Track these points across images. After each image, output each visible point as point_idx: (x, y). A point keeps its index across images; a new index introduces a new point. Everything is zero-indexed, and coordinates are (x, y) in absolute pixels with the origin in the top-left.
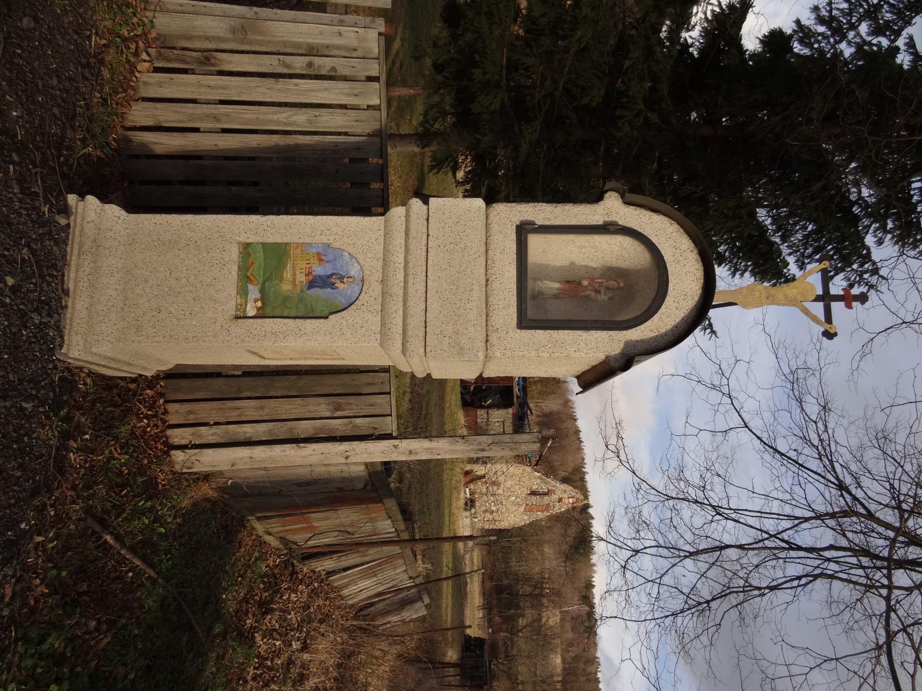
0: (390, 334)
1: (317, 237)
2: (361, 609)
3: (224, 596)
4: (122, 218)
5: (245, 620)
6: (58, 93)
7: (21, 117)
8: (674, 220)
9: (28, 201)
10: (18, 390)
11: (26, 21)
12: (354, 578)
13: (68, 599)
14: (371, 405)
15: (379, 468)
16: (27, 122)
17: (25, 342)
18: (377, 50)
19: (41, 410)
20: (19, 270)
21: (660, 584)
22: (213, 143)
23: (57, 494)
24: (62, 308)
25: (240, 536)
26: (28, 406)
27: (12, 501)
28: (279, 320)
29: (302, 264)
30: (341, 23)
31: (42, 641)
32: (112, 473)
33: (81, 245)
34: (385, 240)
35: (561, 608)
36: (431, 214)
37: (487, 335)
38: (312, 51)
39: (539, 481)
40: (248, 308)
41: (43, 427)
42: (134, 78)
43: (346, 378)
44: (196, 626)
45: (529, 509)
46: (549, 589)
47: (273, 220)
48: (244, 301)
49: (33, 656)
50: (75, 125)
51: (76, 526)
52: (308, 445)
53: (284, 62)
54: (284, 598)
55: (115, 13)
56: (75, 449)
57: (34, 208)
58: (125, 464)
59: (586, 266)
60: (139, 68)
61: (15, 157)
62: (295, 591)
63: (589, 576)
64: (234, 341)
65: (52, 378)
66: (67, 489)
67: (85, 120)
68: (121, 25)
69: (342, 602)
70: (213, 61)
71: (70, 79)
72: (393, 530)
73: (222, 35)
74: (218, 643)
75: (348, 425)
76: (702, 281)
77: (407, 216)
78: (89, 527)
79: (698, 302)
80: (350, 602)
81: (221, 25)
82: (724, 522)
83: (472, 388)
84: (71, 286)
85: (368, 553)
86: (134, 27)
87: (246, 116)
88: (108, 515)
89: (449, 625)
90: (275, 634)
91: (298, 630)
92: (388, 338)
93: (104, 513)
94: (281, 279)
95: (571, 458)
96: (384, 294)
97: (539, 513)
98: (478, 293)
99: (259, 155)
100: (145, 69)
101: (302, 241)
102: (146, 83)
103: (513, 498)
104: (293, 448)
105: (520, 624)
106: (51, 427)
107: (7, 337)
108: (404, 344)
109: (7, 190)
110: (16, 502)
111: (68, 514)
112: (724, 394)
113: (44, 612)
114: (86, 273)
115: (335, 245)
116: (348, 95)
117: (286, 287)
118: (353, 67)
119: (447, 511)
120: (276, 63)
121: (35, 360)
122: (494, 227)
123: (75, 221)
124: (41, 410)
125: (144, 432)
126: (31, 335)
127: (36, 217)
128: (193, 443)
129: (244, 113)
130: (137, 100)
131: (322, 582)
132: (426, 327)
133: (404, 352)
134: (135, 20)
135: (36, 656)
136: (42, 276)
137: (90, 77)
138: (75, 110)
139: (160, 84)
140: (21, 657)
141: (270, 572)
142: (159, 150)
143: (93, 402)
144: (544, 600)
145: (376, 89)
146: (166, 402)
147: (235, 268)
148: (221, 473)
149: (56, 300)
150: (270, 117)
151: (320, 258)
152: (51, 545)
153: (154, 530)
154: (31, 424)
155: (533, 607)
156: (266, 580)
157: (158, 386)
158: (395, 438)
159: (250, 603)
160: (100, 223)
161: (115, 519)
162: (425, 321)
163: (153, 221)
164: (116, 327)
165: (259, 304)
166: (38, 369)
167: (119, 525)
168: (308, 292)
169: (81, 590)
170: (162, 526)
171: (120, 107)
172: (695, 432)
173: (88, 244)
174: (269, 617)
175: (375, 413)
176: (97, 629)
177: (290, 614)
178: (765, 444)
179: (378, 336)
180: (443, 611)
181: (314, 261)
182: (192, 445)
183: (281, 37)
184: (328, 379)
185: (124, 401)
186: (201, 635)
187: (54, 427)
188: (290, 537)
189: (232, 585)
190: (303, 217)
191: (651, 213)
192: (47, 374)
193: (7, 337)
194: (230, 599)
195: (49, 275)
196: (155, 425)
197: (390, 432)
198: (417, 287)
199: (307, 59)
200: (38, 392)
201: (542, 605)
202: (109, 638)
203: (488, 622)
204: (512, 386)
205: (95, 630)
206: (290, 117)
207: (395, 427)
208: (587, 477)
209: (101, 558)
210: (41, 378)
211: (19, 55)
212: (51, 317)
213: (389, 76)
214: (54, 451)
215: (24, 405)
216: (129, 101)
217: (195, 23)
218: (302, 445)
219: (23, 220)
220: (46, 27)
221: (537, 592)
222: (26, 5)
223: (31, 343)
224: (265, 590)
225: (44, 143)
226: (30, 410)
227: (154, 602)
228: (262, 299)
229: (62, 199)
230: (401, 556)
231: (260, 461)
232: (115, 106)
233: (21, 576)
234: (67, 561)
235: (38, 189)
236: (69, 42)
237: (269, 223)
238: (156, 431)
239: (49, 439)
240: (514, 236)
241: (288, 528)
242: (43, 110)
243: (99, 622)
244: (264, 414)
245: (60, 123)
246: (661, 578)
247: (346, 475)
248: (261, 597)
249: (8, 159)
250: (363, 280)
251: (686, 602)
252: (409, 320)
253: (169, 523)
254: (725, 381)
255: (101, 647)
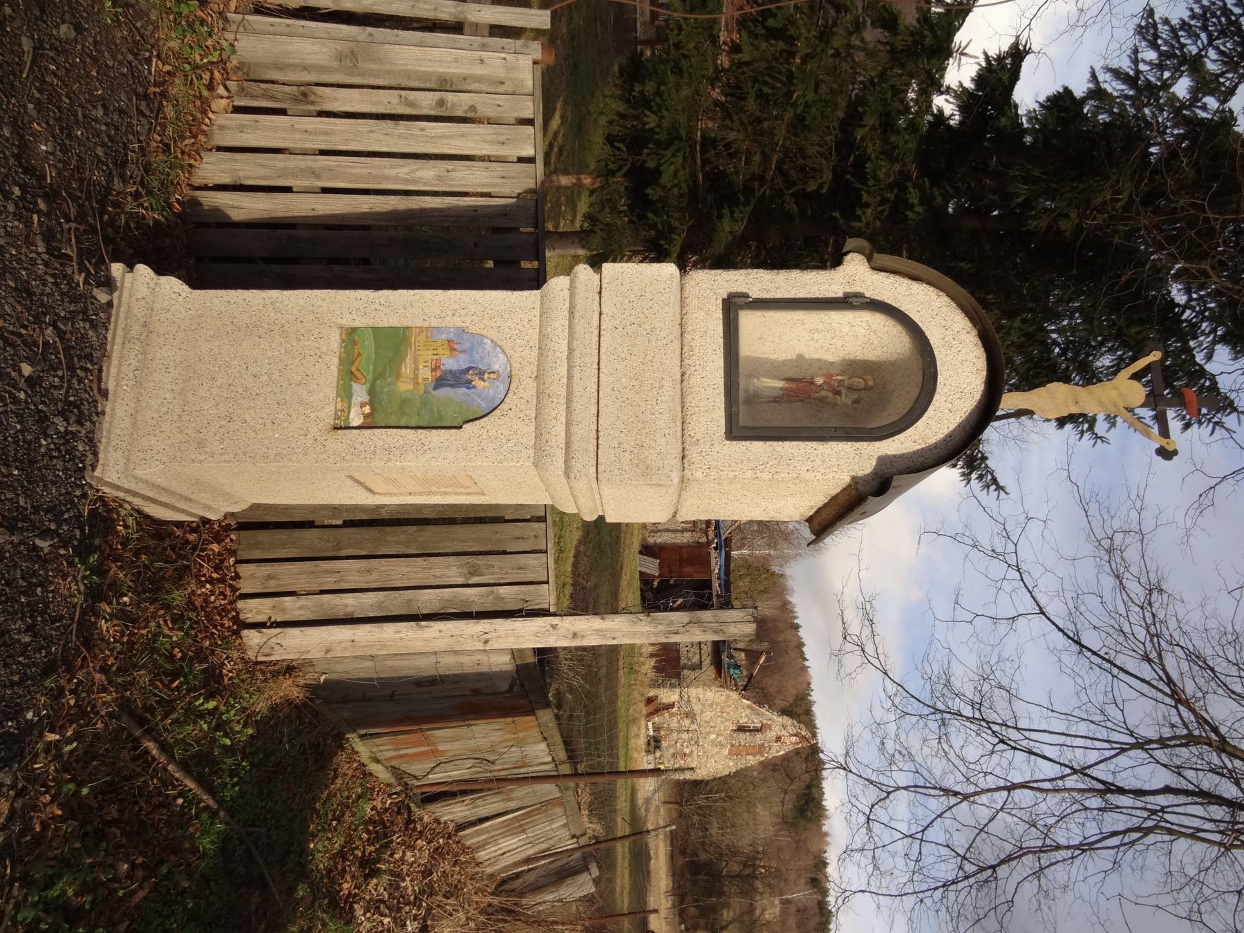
0: (548, 448)
1: (449, 318)
2: (504, 882)
3: (312, 846)
4: (184, 295)
5: (341, 884)
6: (103, 128)
7: (52, 154)
8: (942, 290)
9: (58, 266)
10: (30, 520)
11: (64, 28)
12: (493, 834)
13: (89, 828)
14: (521, 568)
15: (531, 659)
16: (60, 161)
17: (43, 456)
18: (530, 83)
19: (62, 552)
20: (39, 357)
21: (922, 840)
22: (309, 207)
23: (80, 675)
24: (97, 414)
25: (336, 760)
26: (44, 544)
27: (16, 678)
28: (395, 430)
29: (427, 355)
30: (484, 47)
31: (50, 883)
32: (160, 655)
33: (127, 331)
34: (541, 321)
35: (781, 895)
36: (604, 286)
37: (684, 449)
38: (444, 85)
39: (748, 711)
40: (352, 415)
41: (64, 577)
42: (207, 120)
43: (485, 530)
44: (271, 884)
45: (736, 751)
46: (764, 867)
47: (388, 296)
48: (346, 405)
49: (35, 905)
50: (125, 174)
51: (106, 725)
52: (431, 623)
53: (406, 99)
54: (397, 856)
55: (184, 31)
56: (109, 614)
57: (65, 276)
58: (178, 644)
59: (819, 360)
60: (214, 107)
61: (42, 205)
62: (411, 847)
63: (820, 850)
64: (331, 460)
65: (79, 510)
66: (95, 670)
67: (139, 170)
68: (191, 48)
69: (477, 869)
70: (312, 98)
71: (121, 112)
72: (549, 759)
73: (325, 62)
74: (302, 912)
75: (488, 596)
76: (985, 373)
77: (572, 288)
78: (124, 729)
79: (980, 401)
80: (489, 870)
81: (324, 50)
82: (1009, 754)
83: (656, 583)
84: (111, 386)
85: (514, 795)
86: (207, 51)
87: (355, 171)
88: (152, 714)
89: (626, 911)
90: (382, 906)
91: (415, 905)
92: (544, 454)
93: (146, 711)
94: (398, 375)
95: (792, 682)
96: (539, 394)
97: (750, 757)
98: (670, 390)
99: (371, 223)
100: (222, 108)
101: (426, 324)
102: (222, 127)
103: (713, 736)
104: (412, 627)
105: (725, 917)
106: (75, 577)
107: (18, 446)
108: (567, 462)
109: (28, 248)
110: (22, 681)
111: (94, 706)
112: (1009, 565)
113: (55, 844)
114: (132, 368)
115: (472, 329)
116: (491, 143)
117: (404, 386)
118: (499, 106)
119: (622, 752)
120: (395, 100)
121: (57, 482)
122: (693, 302)
123: (120, 298)
124: (62, 552)
125: (206, 601)
126: (52, 446)
127: (67, 287)
128: (273, 620)
129: (353, 167)
130: (211, 150)
131: (449, 837)
132: (598, 438)
133: (567, 474)
134: (209, 42)
135: (41, 906)
136: (71, 368)
137: (148, 113)
138: (126, 155)
139: (241, 128)
140: (17, 907)
141: (377, 818)
142: (237, 216)
143: (137, 553)
144: (759, 885)
145: (529, 135)
146: (238, 562)
147: (336, 361)
148: (310, 663)
149: (89, 403)
150: (386, 172)
151: (451, 346)
152: (69, 748)
153: (214, 740)
154: (47, 570)
155: (742, 893)
156: (371, 828)
157: (228, 540)
158: (554, 615)
159: (348, 860)
160: (154, 302)
161: (162, 720)
162: (597, 431)
163: (226, 298)
164: (170, 442)
165: (367, 409)
166: (61, 495)
167: (166, 730)
168: (434, 393)
169: (109, 818)
170: (226, 735)
171: (186, 157)
172: (970, 617)
173: (136, 328)
174: (375, 881)
175: (525, 580)
176: (130, 876)
177: (404, 880)
178: (1069, 637)
179: (531, 452)
180: (617, 895)
181: (444, 351)
182: (272, 623)
183: (404, 65)
184: (461, 531)
185: (180, 556)
186: (277, 897)
187: (79, 578)
188: (404, 767)
189: (323, 830)
190: (429, 291)
191: (910, 282)
192: (72, 502)
193: (18, 446)
194: (321, 850)
195: (82, 368)
196: (221, 593)
197: (546, 606)
198: (587, 340)
199: (438, 95)
200: (59, 527)
201: (755, 890)
202: (147, 891)
203: (680, 915)
204: (710, 581)
205: (127, 877)
206: (413, 172)
207: (553, 601)
208: (815, 709)
209: (139, 775)
210: (63, 508)
211: (54, 73)
212: (82, 425)
213: (547, 156)
214: (77, 613)
215: (39, 542)
216: (198, 152)
217: (290, 48)
218: (423, 623)
219: (48, 290)
220: (91, 40)
221: (748, 871)
222: (66, 8)
223: (51, 458)
224: (370, 842)
225: (82, 191)
226: (46, 551)
227: (212, 842)
228: (371, 403)
229: (103, 268)
230: (558, 802)
231: (365, 646)
232: (180, 156)
233: (24, 788)
234: (90, 774)
235: (71, 251)
236: (121, 63)
237: (382, 301)
238: (223, 602)
239: (72, 596)
240: (719, 314)
241: (403, 752)
242: (82, 149)
243: (133, 866)
244: (373, 580)
245: (105, 168)
246: (923, 831)
247: (484, 669)
248: (364, 852)
249: (31, 206)
250: (510, 377)
251: (961, 868)
252: (574, 429)
253: (237, 732)
254: (1011, 548)
255: (133, 904)
